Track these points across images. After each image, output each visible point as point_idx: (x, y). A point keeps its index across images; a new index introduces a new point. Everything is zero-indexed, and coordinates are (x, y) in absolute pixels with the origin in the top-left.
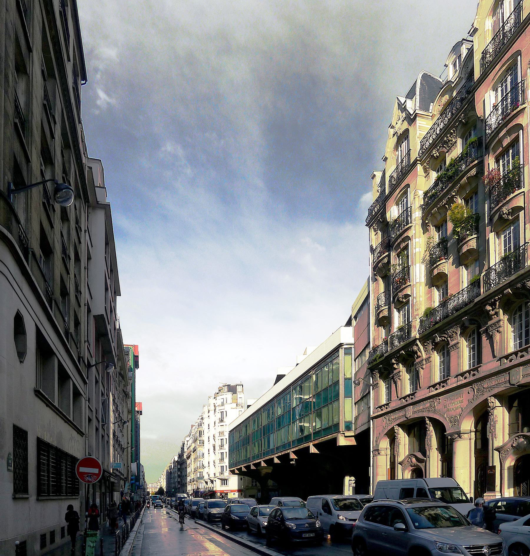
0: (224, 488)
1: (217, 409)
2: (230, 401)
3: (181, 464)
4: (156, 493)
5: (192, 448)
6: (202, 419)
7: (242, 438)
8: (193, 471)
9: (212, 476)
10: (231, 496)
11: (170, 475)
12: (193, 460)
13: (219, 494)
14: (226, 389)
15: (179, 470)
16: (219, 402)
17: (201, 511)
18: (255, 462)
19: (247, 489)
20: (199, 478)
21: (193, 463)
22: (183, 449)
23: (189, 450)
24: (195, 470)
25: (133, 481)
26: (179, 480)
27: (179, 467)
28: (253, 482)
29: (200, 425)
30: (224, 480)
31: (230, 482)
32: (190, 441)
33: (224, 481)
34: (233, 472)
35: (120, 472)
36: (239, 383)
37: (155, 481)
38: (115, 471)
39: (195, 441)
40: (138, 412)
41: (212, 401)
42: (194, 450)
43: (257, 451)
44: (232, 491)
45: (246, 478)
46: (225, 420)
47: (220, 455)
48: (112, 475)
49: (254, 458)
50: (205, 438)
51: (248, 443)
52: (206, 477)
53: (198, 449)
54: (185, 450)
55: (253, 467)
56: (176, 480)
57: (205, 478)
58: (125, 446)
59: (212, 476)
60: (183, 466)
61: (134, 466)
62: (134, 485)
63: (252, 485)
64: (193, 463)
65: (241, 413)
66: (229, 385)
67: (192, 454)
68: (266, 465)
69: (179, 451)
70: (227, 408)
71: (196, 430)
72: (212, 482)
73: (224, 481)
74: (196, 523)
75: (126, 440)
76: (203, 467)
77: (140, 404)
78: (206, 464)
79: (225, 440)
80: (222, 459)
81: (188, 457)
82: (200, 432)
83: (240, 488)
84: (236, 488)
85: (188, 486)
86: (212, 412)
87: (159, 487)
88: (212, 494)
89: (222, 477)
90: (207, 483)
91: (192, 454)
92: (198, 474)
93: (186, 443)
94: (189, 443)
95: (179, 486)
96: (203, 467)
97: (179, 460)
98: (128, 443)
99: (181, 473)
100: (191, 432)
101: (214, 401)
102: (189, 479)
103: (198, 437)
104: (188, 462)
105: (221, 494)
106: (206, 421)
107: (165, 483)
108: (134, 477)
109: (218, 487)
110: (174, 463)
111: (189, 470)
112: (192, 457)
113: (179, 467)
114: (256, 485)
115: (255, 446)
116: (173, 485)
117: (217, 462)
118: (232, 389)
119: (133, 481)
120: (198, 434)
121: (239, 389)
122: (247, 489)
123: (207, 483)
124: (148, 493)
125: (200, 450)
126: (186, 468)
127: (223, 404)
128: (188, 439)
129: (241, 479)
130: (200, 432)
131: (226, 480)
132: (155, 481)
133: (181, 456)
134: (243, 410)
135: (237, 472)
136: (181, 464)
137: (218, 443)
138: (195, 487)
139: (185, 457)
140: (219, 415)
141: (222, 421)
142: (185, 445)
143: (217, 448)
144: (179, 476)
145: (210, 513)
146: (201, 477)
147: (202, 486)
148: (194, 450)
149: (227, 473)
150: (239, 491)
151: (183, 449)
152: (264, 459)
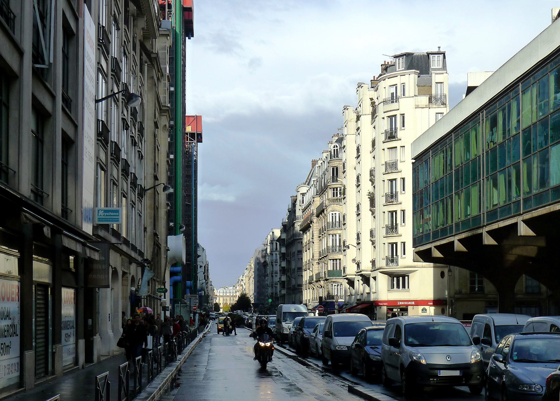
0: (397, 295)
1: (381, 109)
2: (411, 89)
3: (290, 244)
4: (234, 308)
5: (314, 208)
6: (340, 140)
7: (443, 173)
8: (317, 256)
9: (366, 266)
10: (416, 314)
11: (262, 269)
12: (316, 234)
13: (384, 309)
14: (401, 63)
15: (283, 256)
16: (385, 89)
17: (374, 353)
18: (495, 226)
19: (458, 300)
20: (331, 273)
21: (316, 239)
22: (292, 212)
23: (307, 213)
24: (323, 257)
25: (178, 278)
26: (284, 278)
27: (283, 250)
28: (473, 282)
29: (335, 155)
30: (398, 277)
31: (413, 280)
32: (309, 193)
33: (399, 279)
34: (425, 256)
35: (134, 248)
36: (436, 50)
37: (230, 283)
38: (102, 233)
39: (322, 191)
40: (192, 135)
41: (368, 94)
42: (321, 212)
43: (503, 198)
44: (418, 303)
45: (456, 270)
46: (400, 134)
47: (387, 216)
48: (92, 242)
49: (493, 216)
50: (348, 181)
51: (474, 178)
52: (351, 270)
53: (329, 209)
54: (299, 213)
55: (488, 241)
56: (277, 279)
57: (348, 271)
58: (145, 181)
59: (366, 266)
60: (294, 249)
61: (176, 244)
62: (180, 285)
63: (472, 289)
64: (316, 239)
65: (440, 117)
66: (408, 55)
67: (315, 219)
68: (531, 233)
69: (284, 217)
70: (405, 106)
71: (325, 166)
72: (366, 280)
73: (399, 279)
74: (352, 391)
75: (150, 170)
76: (344, 247)
77: (197, 119)
78: (351, 240)
79: (399, 182)
80: (392, 228)
81: (306, 228)
82: (335, 171)
83: (439, 297)
84: (429, 295)
85: (305, 292)
86: (366, 119)
87: (238, 294)
88: (369, 307)
89: (393, 268)
90: (351, 283)
91: (315, 219)
92: (330, 263)
93: (300, 198)
94: (307, 199)
95: (284, 292)
96: (344, 247)
97: (284, 236)
98: (156, 178)
99: (289, 263)
100: (311, 175)
101: (372, 94)
102: (306, 276)
103: (330, 182)
104: (306, 238)
105: (390, 309)
106: (350, 143)
107: (252, 287)
108: (179, 269)
109: (382, 291)
110: (272, 243)
111: (306, 257)
112: (316, 227)
113: (283, 250)
114: (481, 289)
115: (495, 185)
116: (270, 291)
117: (381, 233)
118: (419, 63)
119: (178, 278)
120: (330, 175)
121: (435, 62)
122: (458, 300)
123: (351, 283)
124: (217, 307)
125: (333, 211)
126: (300, 252)
127: (394, 98)
128: (304, 190)
129: (442, 275)
130: (335, 171)
131: (404, 277)
132: (230, 283)
133: (287, 228)
134: (444, 110)
135: (437, 254)
136: (290, 244)
137: (382, 190)
138: (323, 293)
139: (298, 227)
140: (384, 125)
141: (391, 136)
142: (298, 203)
143: (380, 200)
144: (283, 271)
145: (415, 364)
146: (337, 272)
147: (340, 291)
148: (321, 212)
149: (407, 259)
150: (437, 302)
151: (292, 212)
152: (527, 216)
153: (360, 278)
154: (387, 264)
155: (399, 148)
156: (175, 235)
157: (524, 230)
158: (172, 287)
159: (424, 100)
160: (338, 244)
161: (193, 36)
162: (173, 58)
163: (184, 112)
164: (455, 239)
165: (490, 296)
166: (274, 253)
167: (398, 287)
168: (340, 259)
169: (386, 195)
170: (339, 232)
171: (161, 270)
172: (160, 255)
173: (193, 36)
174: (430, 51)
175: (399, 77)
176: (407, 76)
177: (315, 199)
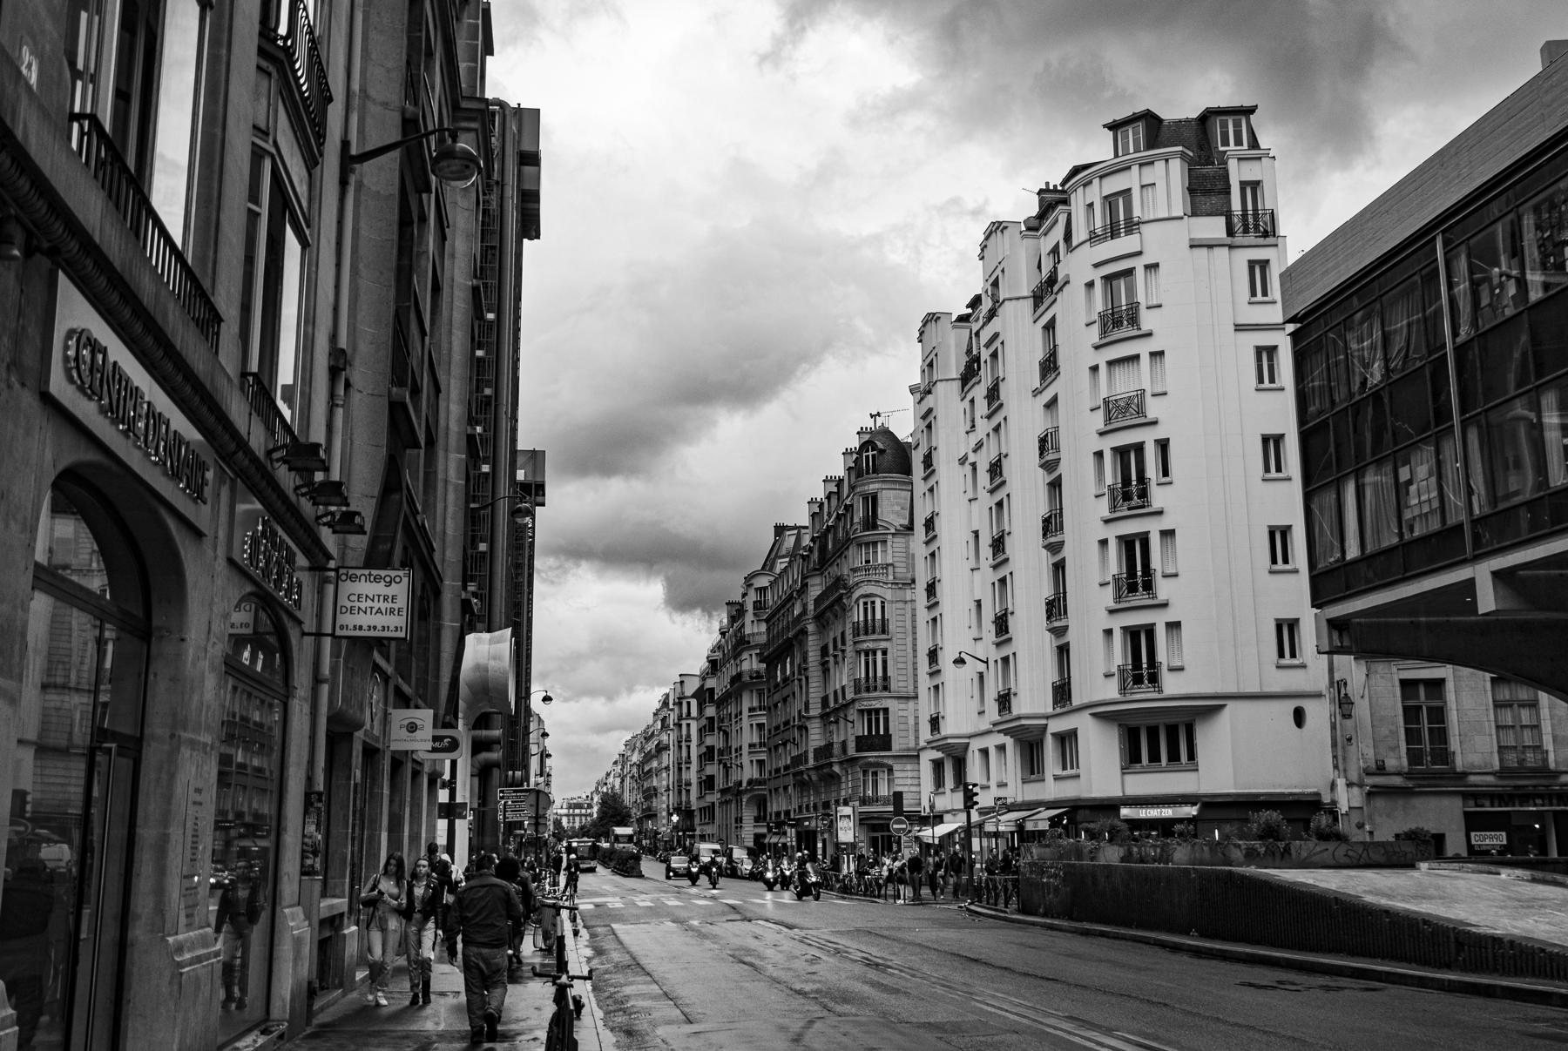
25: (495, 755)
77: (536, 457)
119: (495, 755)
153: (1009, 741)
154: (1123, 689)
155: (1145, 359)
156: (489, 631)
157: (1487, 600)
158: (476, 780)
159: (1214, 227)
160: (880, 673)
161: (538, 237)
162: (493, 248)
163: (514, 440)
164: (1482, 573)
165: (1472, 779)
166: (684, 723)
167: (1154, 757)
168: (886, 710)
169: (1112, 490)
170: (883, 645)
171: (437, 677)
172: (439, 616)
173: (538, 237)
174: (1214, 104)
175: (1135, 168)
176: (1160, 165)
177: (810, 581)
